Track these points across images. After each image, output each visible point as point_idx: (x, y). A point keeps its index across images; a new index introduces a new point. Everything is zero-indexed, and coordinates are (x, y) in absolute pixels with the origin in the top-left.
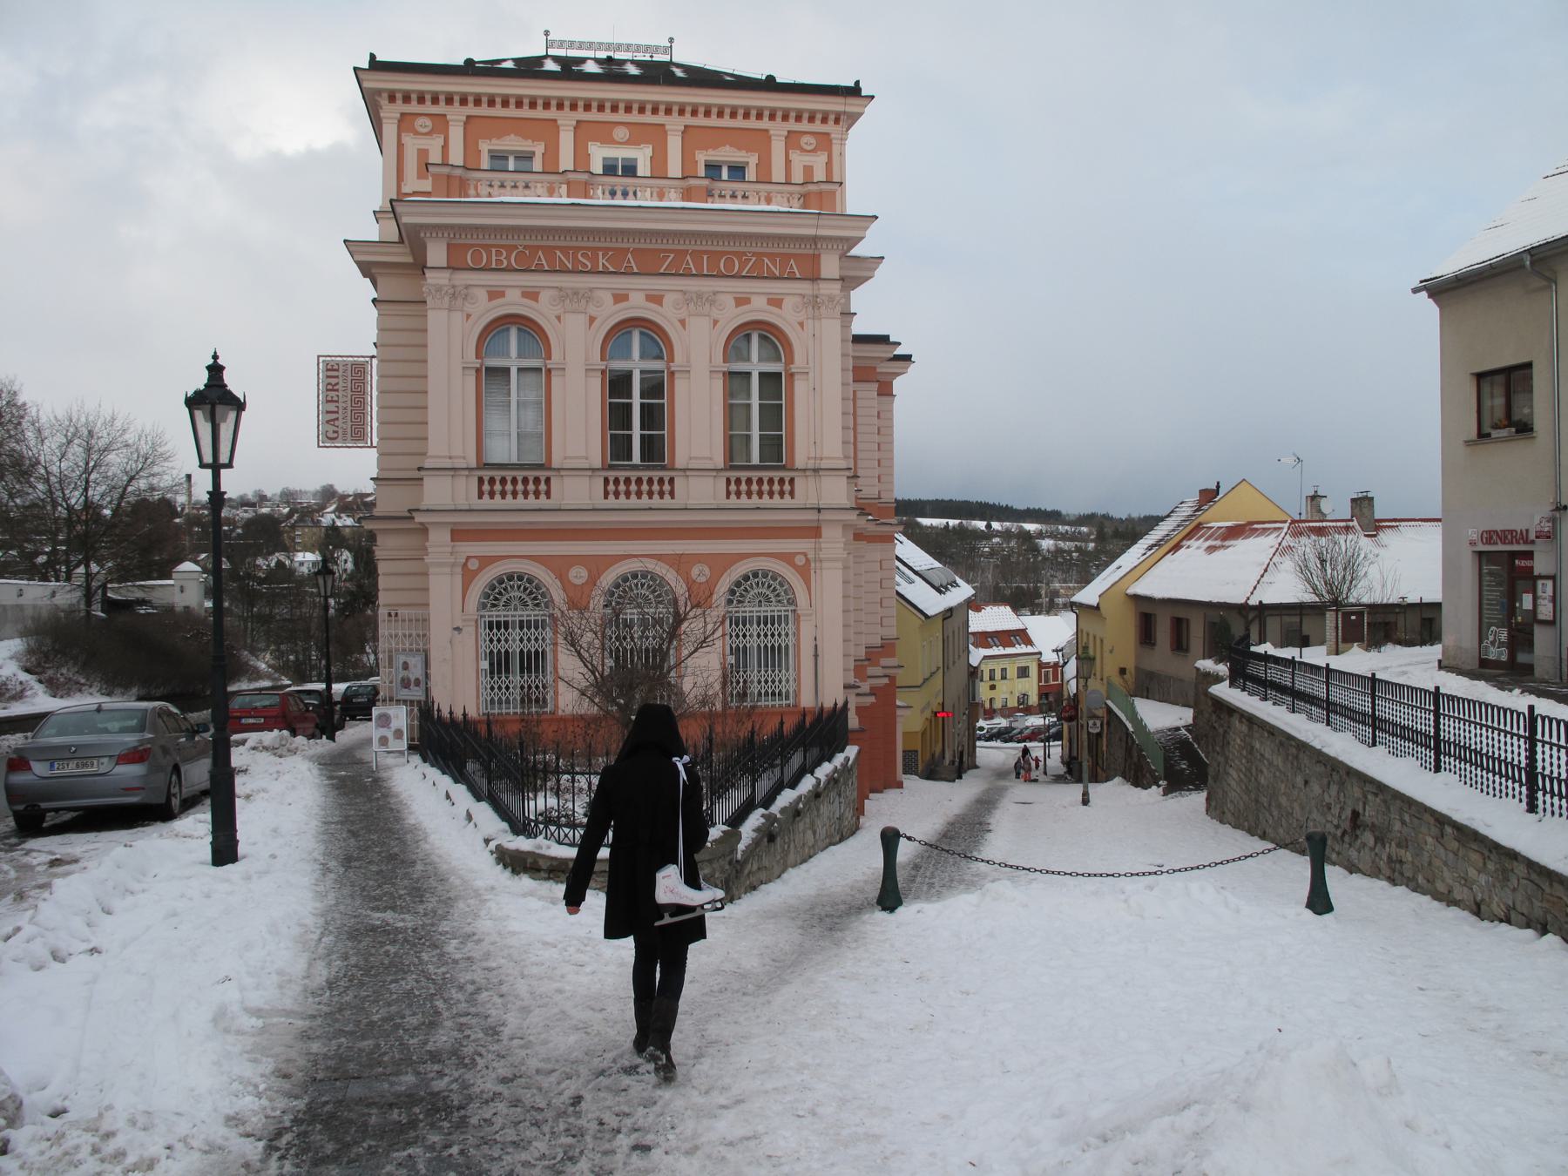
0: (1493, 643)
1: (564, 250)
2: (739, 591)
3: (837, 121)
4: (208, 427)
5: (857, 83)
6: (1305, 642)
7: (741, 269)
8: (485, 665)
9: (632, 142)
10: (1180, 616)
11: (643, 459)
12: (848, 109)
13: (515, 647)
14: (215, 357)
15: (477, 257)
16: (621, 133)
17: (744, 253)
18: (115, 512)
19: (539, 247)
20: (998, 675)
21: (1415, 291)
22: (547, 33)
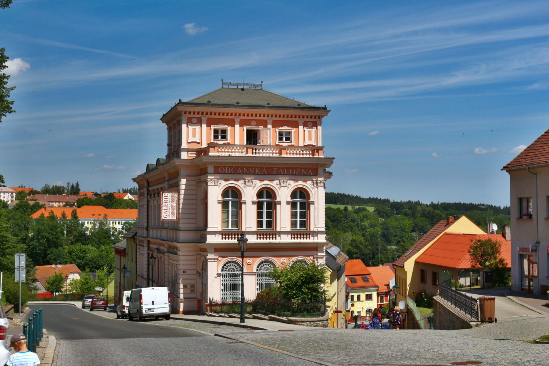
5: (326, 106)
7: (296, 172)
15: (222, 170)
16: (254, 123)
18: (92, 233)
20: (355, 299)
22: (222, 80)
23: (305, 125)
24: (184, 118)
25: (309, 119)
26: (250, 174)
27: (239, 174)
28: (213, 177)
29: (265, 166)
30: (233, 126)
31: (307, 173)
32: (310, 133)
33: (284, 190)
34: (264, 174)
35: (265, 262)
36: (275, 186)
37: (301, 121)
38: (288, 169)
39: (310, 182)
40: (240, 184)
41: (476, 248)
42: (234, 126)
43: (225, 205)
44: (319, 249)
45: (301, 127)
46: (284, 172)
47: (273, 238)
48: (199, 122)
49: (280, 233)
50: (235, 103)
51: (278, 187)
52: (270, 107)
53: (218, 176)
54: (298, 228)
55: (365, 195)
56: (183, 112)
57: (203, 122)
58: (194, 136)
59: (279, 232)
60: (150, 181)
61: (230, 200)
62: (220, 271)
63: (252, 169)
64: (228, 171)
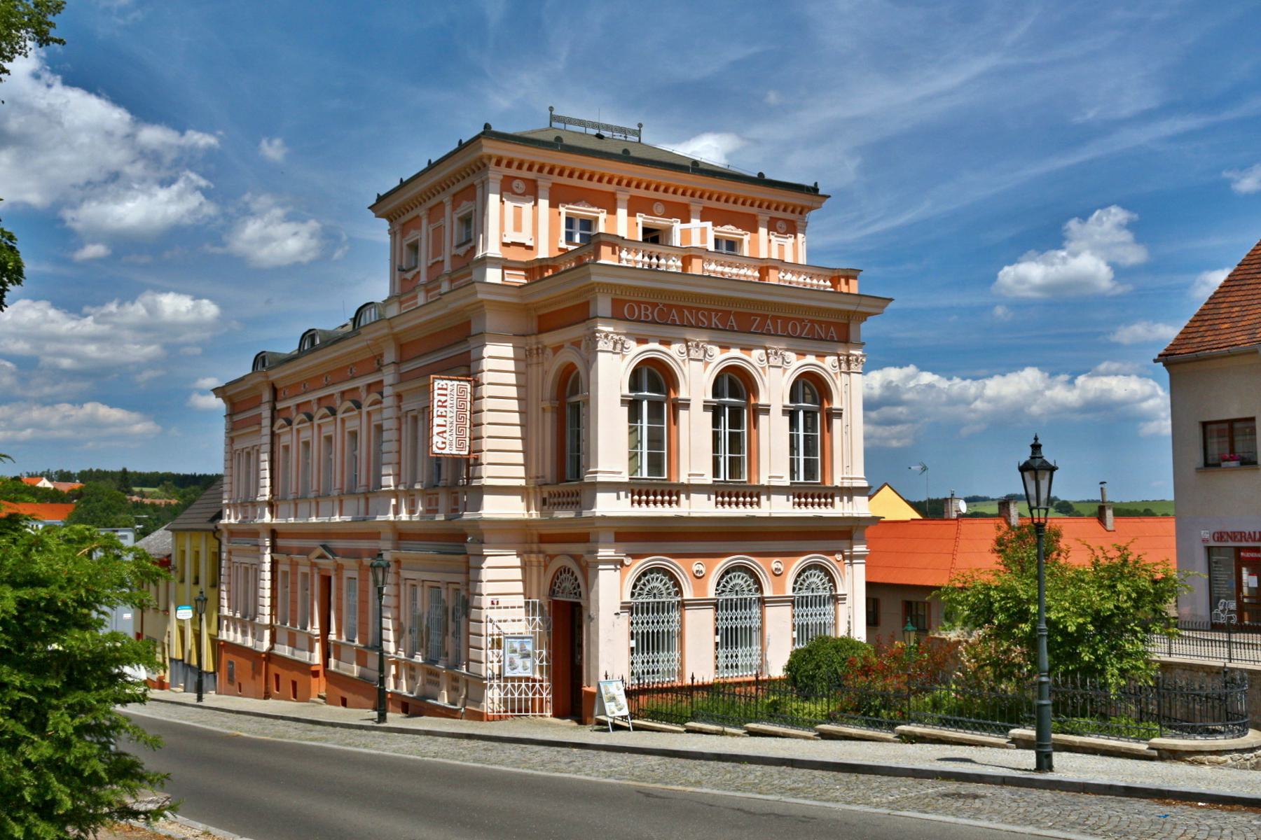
0: (1223, 611)
1: (690, 309)
4: (1034, 483)
9: (668, 214)
10: (908, 599)
14: (1036, 439)
19: (831, 323)
21: (1155, 361)
22: (551, 109)
23: (772, 227)
24: (495, 175)
25: (780, 214)
26: (698, 326)
27: (674, 324)
28: (611, 329)
29: (734, 309)
31: (827, 334)
32: (769, 251)
35: (651, 571)
36: (756, 364)
37: (763, 217)
38: (786, 320)
39: (830, 361)
40: (674, 353)
43: (633, 407)
45: (763, 231)
48: (532, 192)
50: (620, 152)
51: (763, 368)
52: (625, 157)
53: (623, 327)
57: (540, 193)
58: (518, 228)
59: (768, 487)
60: (278, 386)
62: (627, 598)
63: (703, 315)
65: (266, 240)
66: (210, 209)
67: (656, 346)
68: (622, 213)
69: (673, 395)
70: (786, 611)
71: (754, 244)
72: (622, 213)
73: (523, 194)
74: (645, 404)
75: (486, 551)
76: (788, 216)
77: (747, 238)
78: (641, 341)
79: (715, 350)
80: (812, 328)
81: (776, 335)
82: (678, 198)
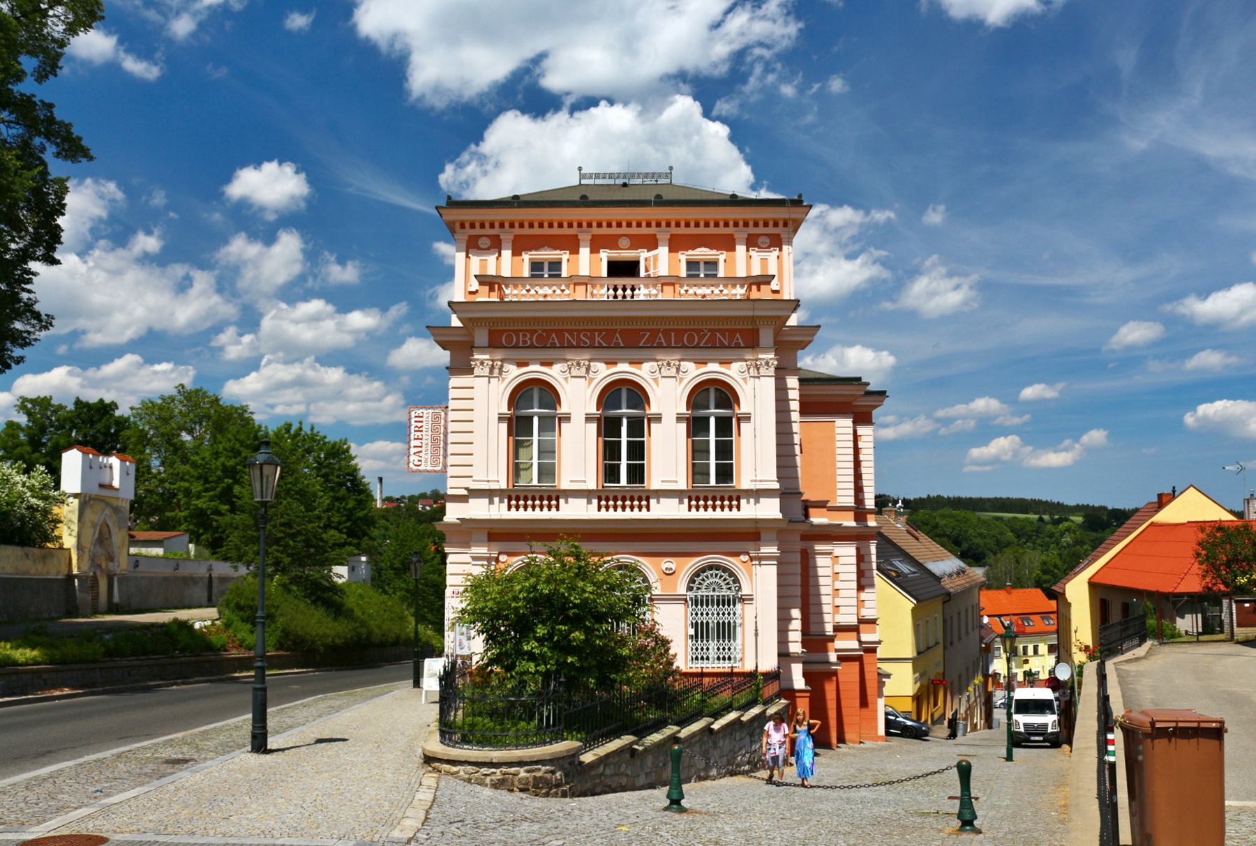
1: (570, 332)
2: (698, 580)
3: (785, 225)
6: (1222, 622)
8: (692, 632)
11: (629, 482)
12: (793, 216)
13: (712, 621)
16: (624, 242)
17: (702, 330)
19: (552, 331)
22: (580, 169)
23: (751, 243)
25: (761, 230)
26: (579, 346)
27: (553, 346)
28: (487, 357)
29: (619, 327)
30: (575, 251)
33: (668, 387)
34: (617, 346)
35: (711, 567)
37: (741, 234)
38: (679, 333)
41: (1214, 545)
42: (577, 252)
44: (763, 536)
45: (740, 249)
46: (669, 342)
47: (640, 508)
49: (660, 494)
52: (660, 202)
54: (713, 482)
55: (1071, 502)
56: (458, 225)
57: (503, 245)
61: (536, 414)
64: (525, 342)
65: (932, 294)
66: (887, 274)
67: (537, 367)
68: (585, 251)
69: (737, 411)
70: (679, 609)
71: (730, 263)
72: (585, 251)
73: (488, 249)
74: (625, 421)
75: (447, 550)
76: (771, 230)
77: (722, 257)
78: (521, 364)
79: (600, 366)
80: (713, 335)
81: (669, 347)
82: (644, 230)
